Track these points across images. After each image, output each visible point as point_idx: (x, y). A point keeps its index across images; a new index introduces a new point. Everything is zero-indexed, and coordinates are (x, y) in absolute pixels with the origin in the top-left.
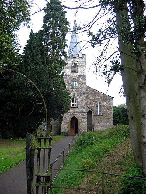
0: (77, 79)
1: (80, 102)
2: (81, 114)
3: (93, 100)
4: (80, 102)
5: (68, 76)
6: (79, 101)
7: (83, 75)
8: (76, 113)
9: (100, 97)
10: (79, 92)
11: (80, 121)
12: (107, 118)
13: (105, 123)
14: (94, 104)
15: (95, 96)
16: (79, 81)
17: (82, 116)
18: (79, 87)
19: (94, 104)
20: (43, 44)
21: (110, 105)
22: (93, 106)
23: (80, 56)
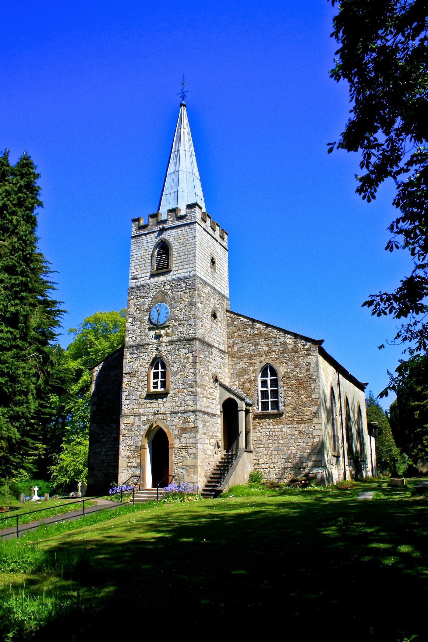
0: (169, 292)
1: (176, 373)
2: (179, 415)
3: (251, 357)
4: (176, 373)
5: (143, 286)
6: (174, 369)
7: (187, 274)
8: (165, 414)
9: (274, 344)
10: (174, 337)
11: (177, 441)
12: (298, 423)
13: (292, 441)
14: (254, 371)
15: (258, 344)
16: (174, 298)
17: (183, 423)
18: (176, 320)
19: (254, 371)
20: (424, 237)
21: (308, 370)
22: (250, 382)
23: (182, 213)
